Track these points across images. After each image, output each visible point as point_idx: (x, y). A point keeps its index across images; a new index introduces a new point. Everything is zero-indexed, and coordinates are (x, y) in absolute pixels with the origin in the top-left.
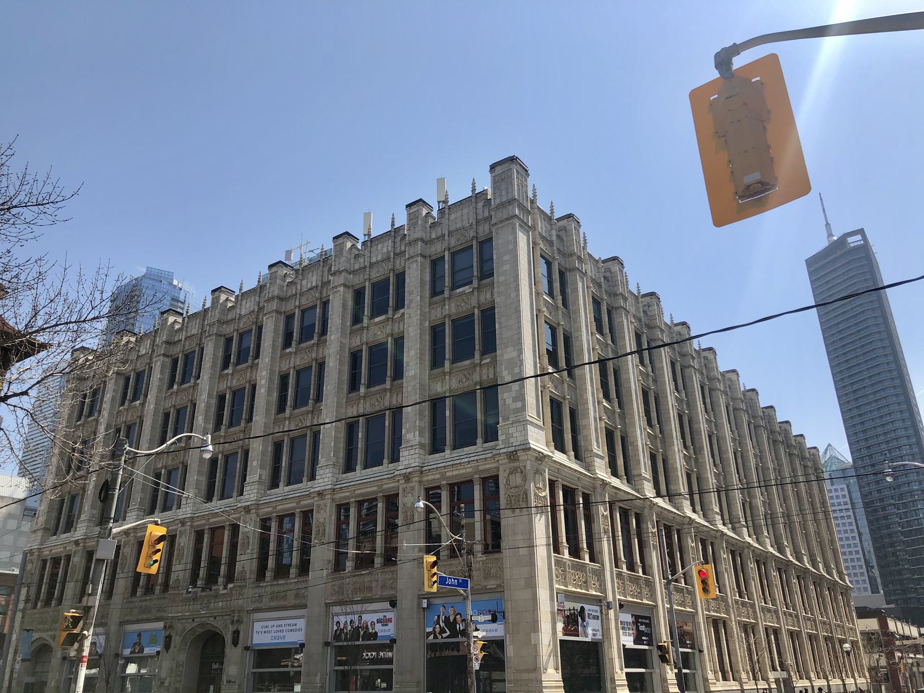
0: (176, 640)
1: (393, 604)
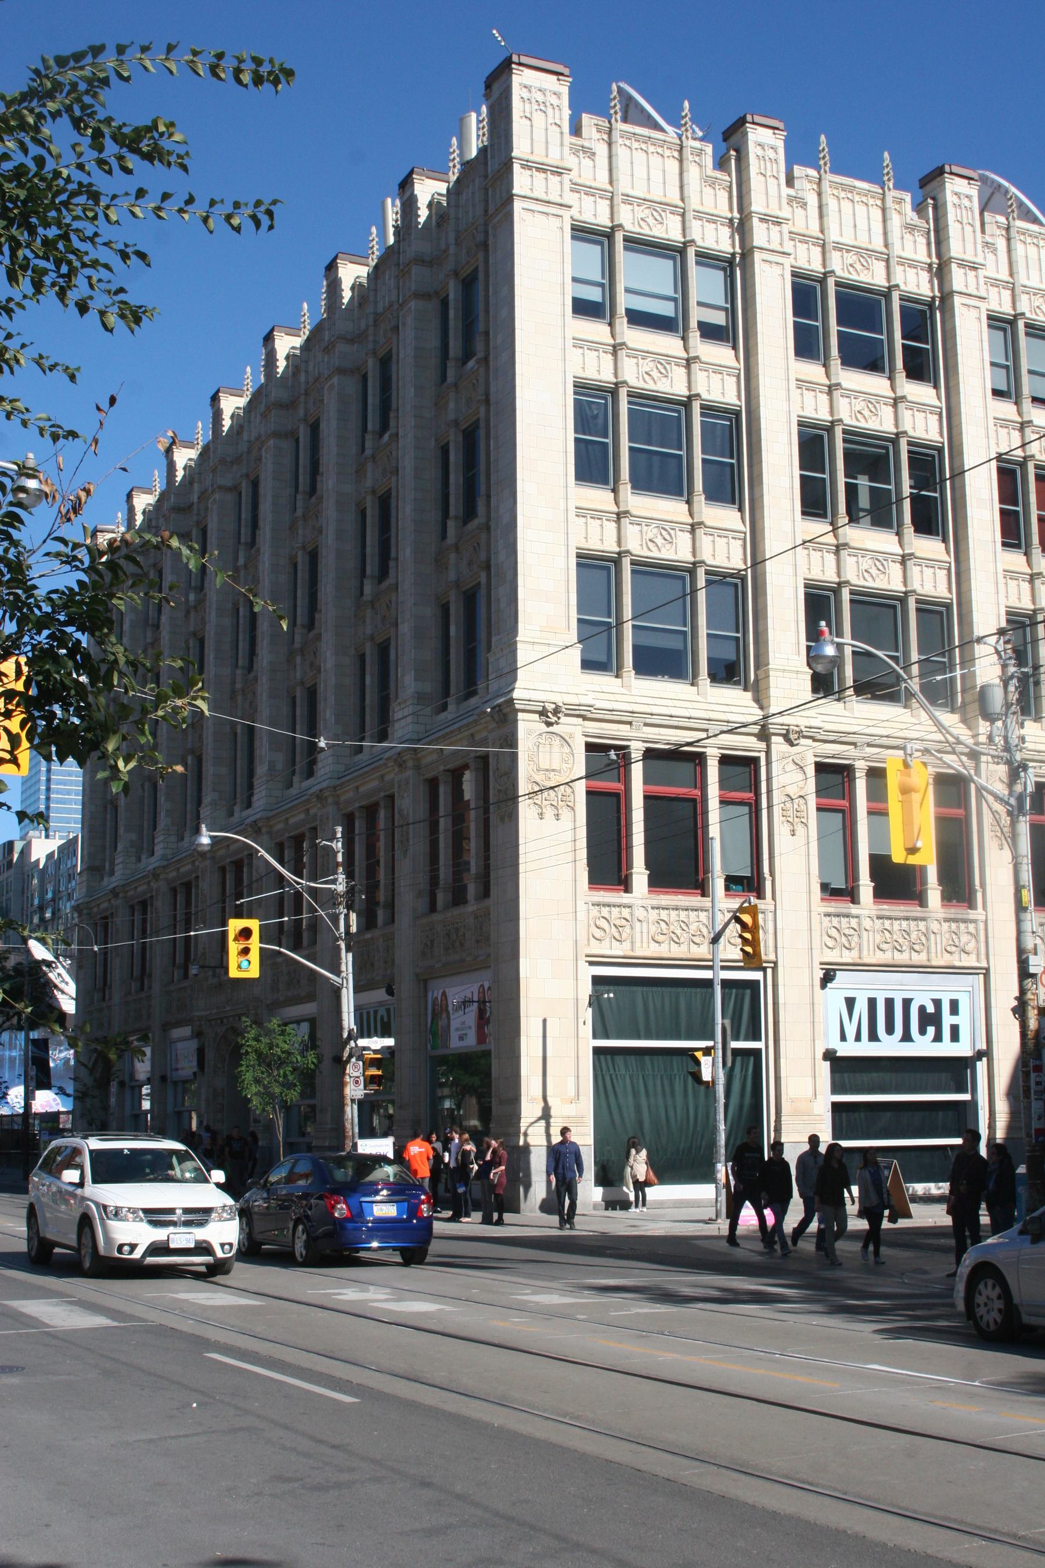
0: (210, 1055)
1: (390, 992)
